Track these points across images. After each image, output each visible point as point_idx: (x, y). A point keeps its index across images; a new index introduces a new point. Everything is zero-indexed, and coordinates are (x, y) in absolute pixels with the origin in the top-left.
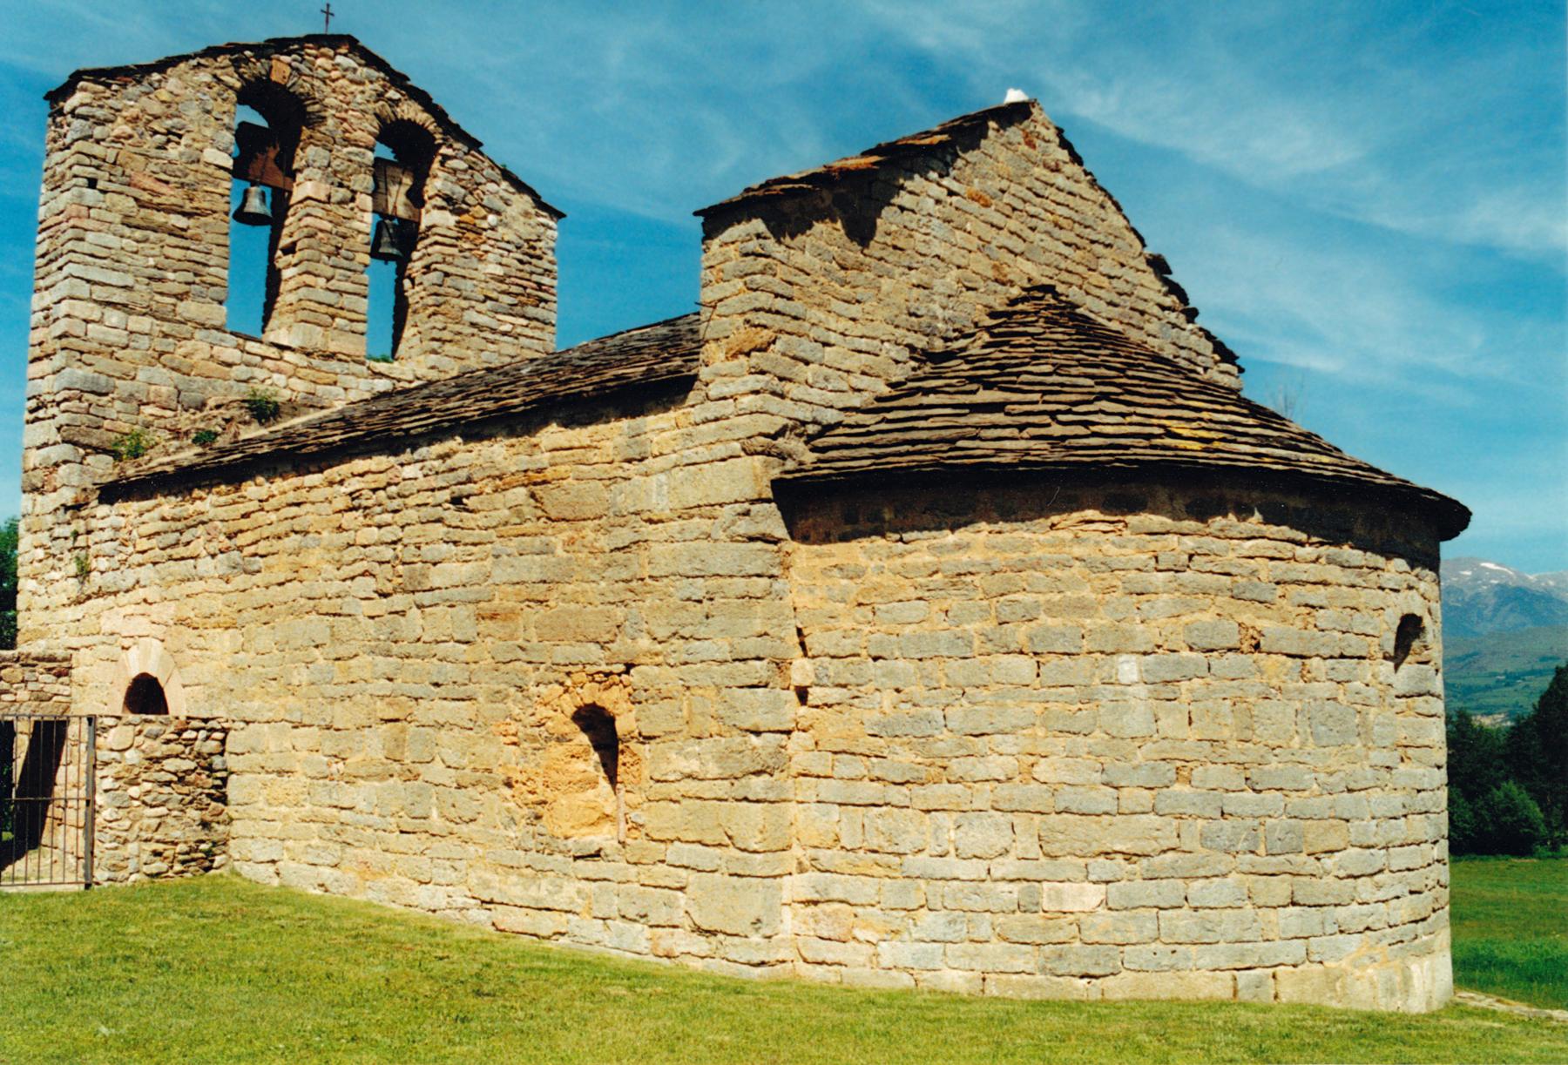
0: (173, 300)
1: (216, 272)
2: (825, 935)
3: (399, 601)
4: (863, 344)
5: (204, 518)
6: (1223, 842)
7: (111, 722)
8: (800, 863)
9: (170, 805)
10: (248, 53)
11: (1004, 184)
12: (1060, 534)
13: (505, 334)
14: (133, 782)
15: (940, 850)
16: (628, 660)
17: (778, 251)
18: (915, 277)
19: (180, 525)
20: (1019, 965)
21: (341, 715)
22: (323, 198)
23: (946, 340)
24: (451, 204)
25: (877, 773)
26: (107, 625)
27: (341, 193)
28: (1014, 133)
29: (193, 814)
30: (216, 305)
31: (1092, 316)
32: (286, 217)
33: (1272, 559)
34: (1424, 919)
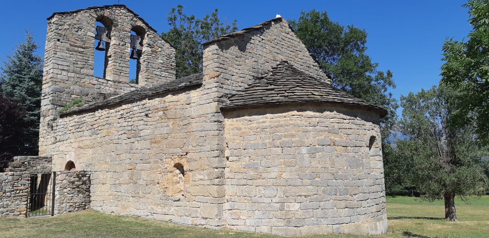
0: (80, 69)
1: (91, 62)
2: (233, 218)
3: (132, 140)
4: (242, 75)
5: (85, 122)
6: (328, 192)
7: (59, 173)
8: (227, 200)
9: (75, 194)
10: (98, 9)
11: (275, 37)
12: (287, 118)
13: (163, 77)
14: (65, 188)
15: (260, 196)
16: (187, 152)
17: (221, 53)
18: (254, 59)
19: (79, 123)
20: (280, 224)
21: (117, 168)
22: (118, 44)
23: (262, 74)
24: (149, 45)
25: (245, 177)
26: (61, 149)
27: (122, 43)
28: (278, 25)
29: (81, 195)
30: (91, 70)
31: (297, 68)
32: (109, 49)
33: (338, 123)
34: (380, 211)
